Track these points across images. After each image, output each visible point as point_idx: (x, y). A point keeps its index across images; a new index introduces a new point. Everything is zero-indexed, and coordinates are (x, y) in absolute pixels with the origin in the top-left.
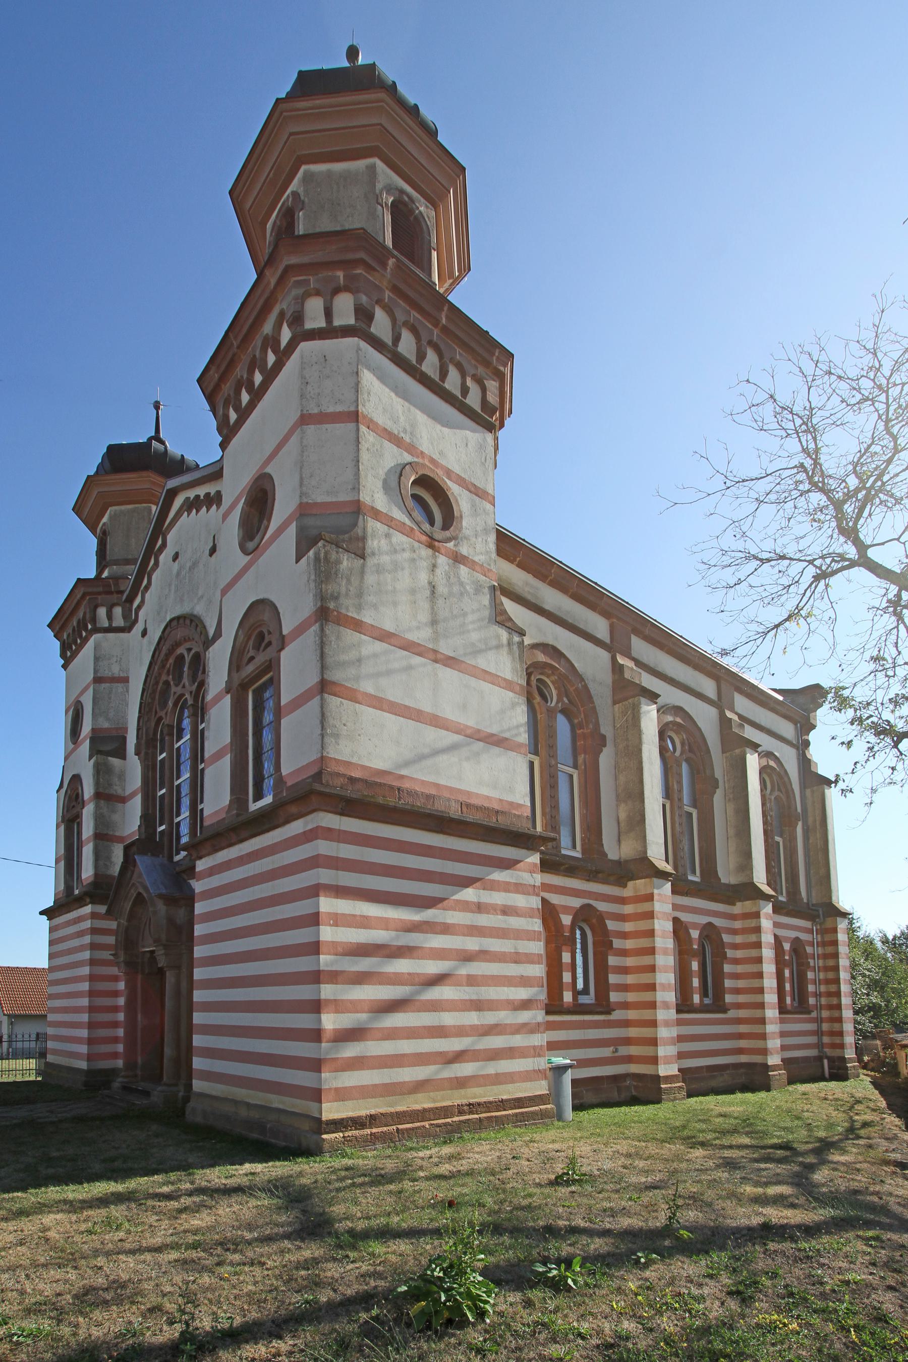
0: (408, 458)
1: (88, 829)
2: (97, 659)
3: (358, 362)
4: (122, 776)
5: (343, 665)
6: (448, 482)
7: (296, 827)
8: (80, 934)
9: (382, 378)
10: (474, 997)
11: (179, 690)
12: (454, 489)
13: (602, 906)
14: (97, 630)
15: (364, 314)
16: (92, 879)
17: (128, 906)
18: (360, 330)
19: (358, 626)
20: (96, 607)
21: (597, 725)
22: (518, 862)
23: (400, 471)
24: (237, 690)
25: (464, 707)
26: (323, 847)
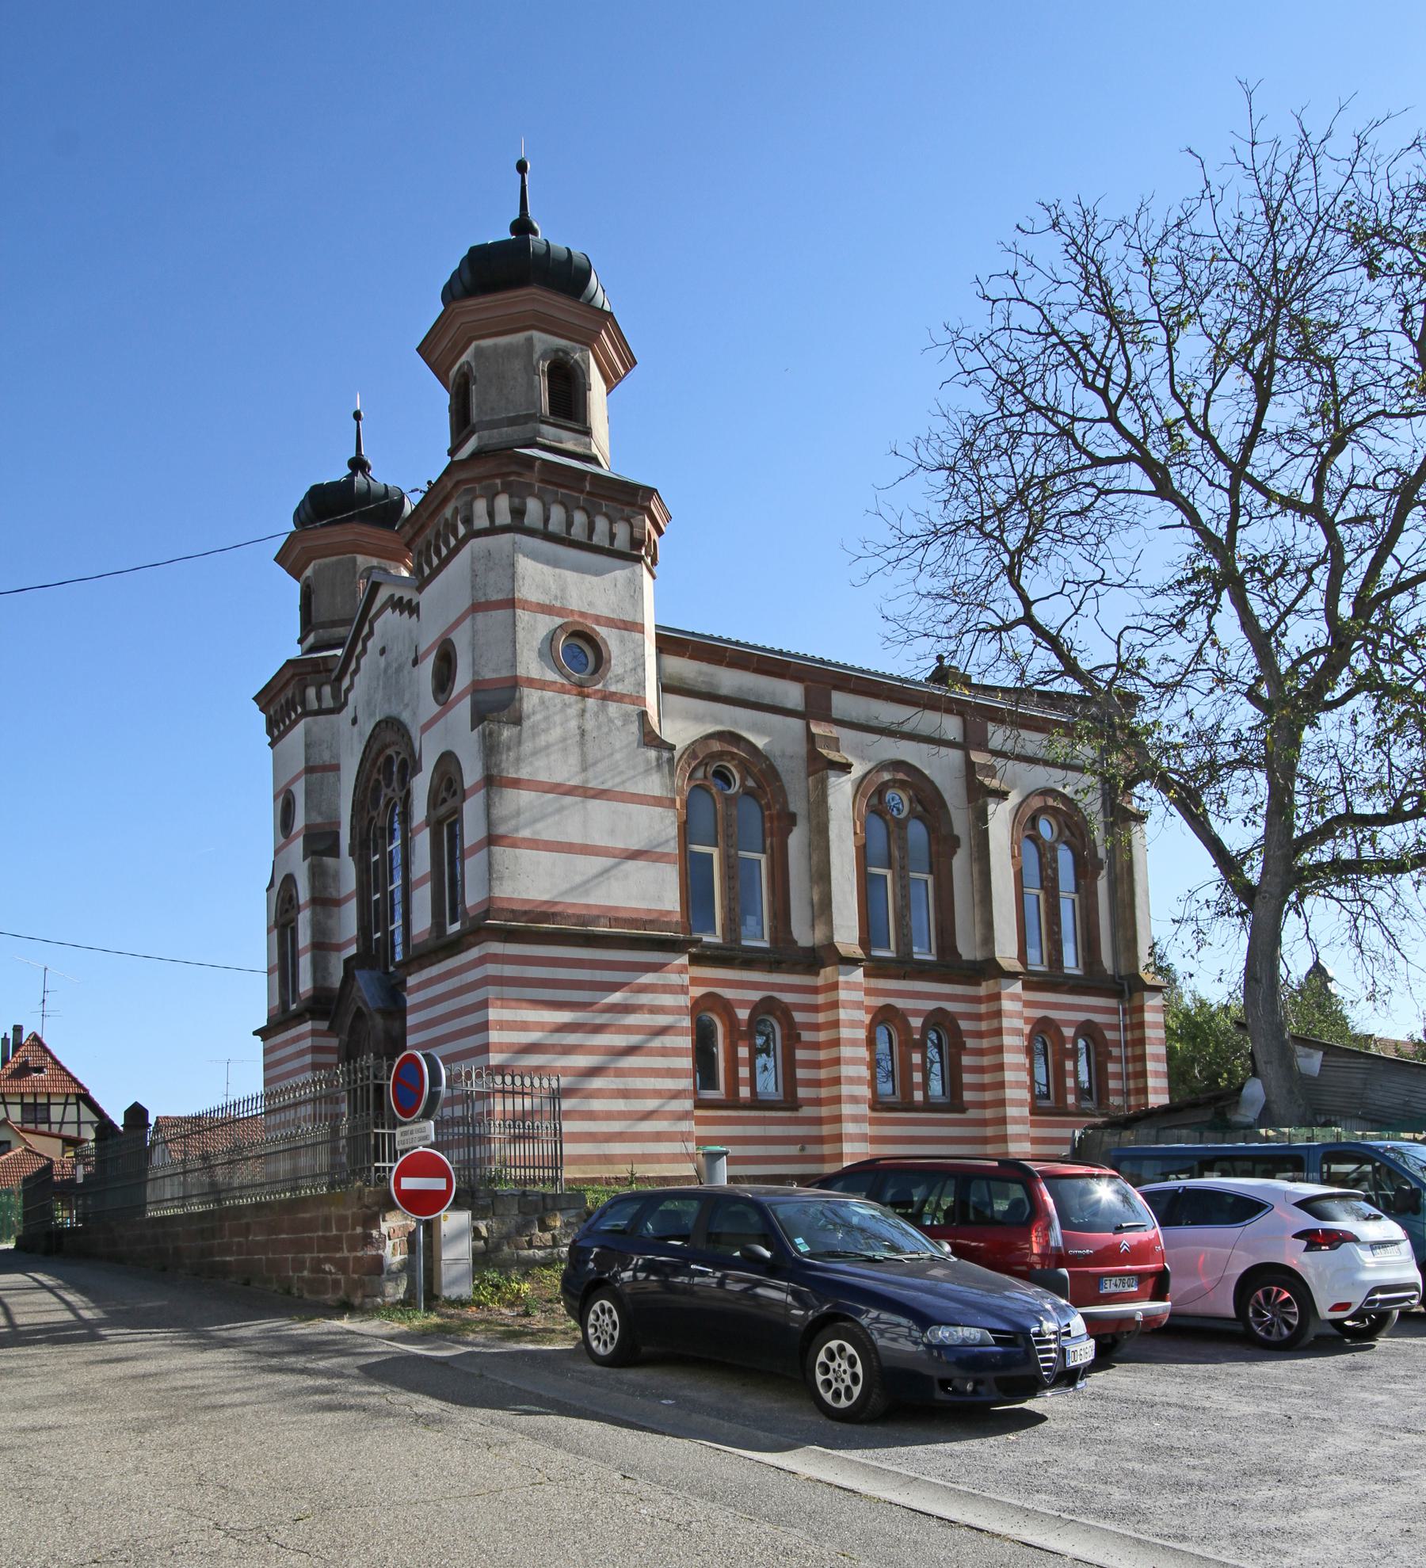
0: (559, 621)
1: (304, 938)
2: (308, 746)
3: (514, 551)
4: (336, 876)
5: (504, 819)
6: (597, 628)
7: (474, 953)
8: (300, 1054)
9: (535, 556)
10: (622, 1087)
11: (390, 793)
12: (602, 631)
13: (787, 998)
14: (306, 713)
15: (518, 513)
16: (310, 993)
17: (349, 1020)
18: (518, 525)
19: (516, 783)
20: (305, 687)
21: (785, 803)
22: (665, 965)
23: (552, 638)
24: (435, 824)
25: (612, 832)
26: (492, 969)
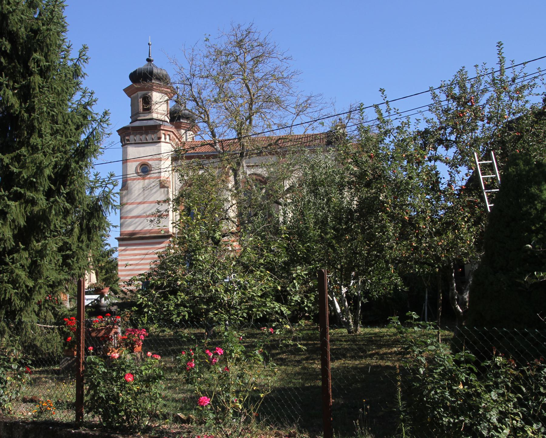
9: (136, 144)
12: (150, 162)
